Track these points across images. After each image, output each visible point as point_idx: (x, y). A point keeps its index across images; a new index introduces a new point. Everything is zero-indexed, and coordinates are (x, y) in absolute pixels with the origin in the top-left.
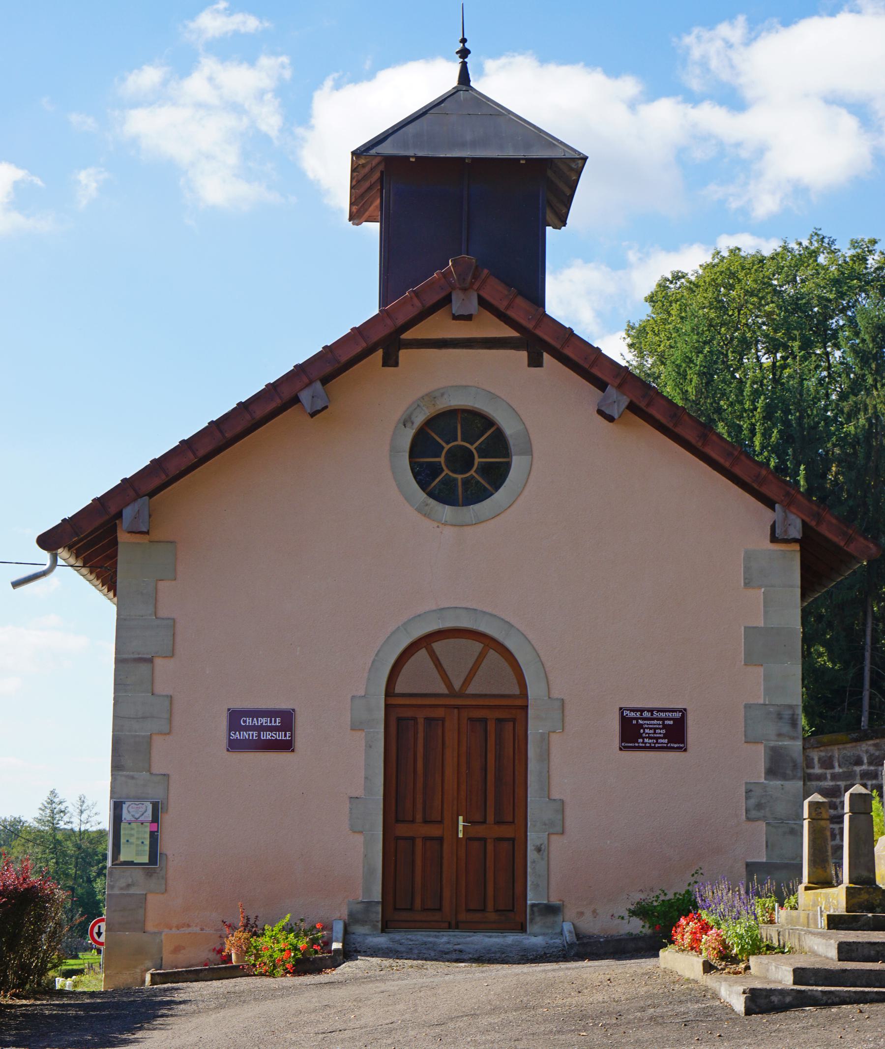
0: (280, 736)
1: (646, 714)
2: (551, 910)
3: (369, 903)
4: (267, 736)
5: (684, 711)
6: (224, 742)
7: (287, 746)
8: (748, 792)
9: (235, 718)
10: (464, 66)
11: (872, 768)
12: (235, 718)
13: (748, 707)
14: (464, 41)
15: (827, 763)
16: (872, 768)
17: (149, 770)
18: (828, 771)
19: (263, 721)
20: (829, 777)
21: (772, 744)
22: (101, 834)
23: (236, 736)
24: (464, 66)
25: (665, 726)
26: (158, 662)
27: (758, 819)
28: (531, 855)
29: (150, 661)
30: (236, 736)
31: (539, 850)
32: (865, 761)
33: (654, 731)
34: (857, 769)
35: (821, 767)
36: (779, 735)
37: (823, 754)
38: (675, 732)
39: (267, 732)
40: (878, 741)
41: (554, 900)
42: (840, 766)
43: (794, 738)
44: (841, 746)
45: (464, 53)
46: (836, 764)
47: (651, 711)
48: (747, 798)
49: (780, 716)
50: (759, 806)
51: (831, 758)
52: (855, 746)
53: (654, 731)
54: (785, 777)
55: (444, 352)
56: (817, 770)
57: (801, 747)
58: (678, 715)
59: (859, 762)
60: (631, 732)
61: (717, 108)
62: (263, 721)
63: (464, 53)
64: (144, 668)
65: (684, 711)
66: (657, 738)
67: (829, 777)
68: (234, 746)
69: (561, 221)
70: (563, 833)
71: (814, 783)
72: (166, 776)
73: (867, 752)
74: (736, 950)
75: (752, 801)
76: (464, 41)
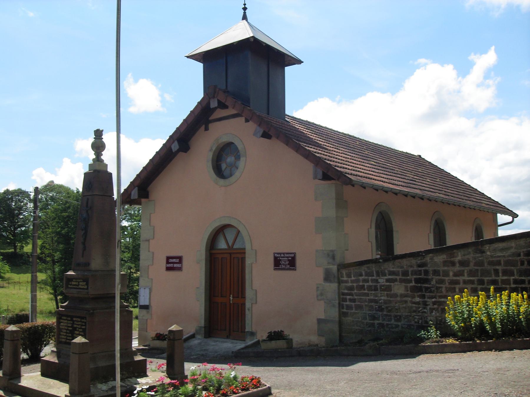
1: (282, 255)
2: (253, 334)
3: (201, 327)
5: (295, 254)
6: (165, 268)
8: (318, 288)
10: (245, 13)
11: (366, 278)
13: (317, 251)
15: (349, 276)
16: (366, 278)
17: (148, 277)
18: (349, 279)
20: (350, 281)
21: (326, 267)
24: (245, 13)
25: (289, 260)
26: (151, 241)
27: (320, 300)
28: (247, 311)
31: (249, 310)
32: (364, 274)
33: (285, 262)
34: (361, 278)
35: (346, 277)
36: (329, 263)
37: (347, 271)
38: (292, 263)
40: (368, 265)
41: (254, 330)
42: (354, 276)
43: (334, 265)
44: (354, 268)
46: (352, 276)
47: (284, 254)
48: (317, 291)
49: (328, 255)
50: (322, 294)
51: (350, 273)
52: (21, 311)
53: (285, 262)
54: (330, 281)
56: (345, 279)
57: (336, 269)
58: (293, 255)
59: (361, 275)
60: (277, 263)
64: (147, 243)
65: (295, 254)
66: (286, 265)
67: (350, 281)
68: (168, 269)
70: (256, 303)
71: (344, 284)
72: (152, 279)
73: (364, 270)
75: (319, 292)
76: (245, 4)
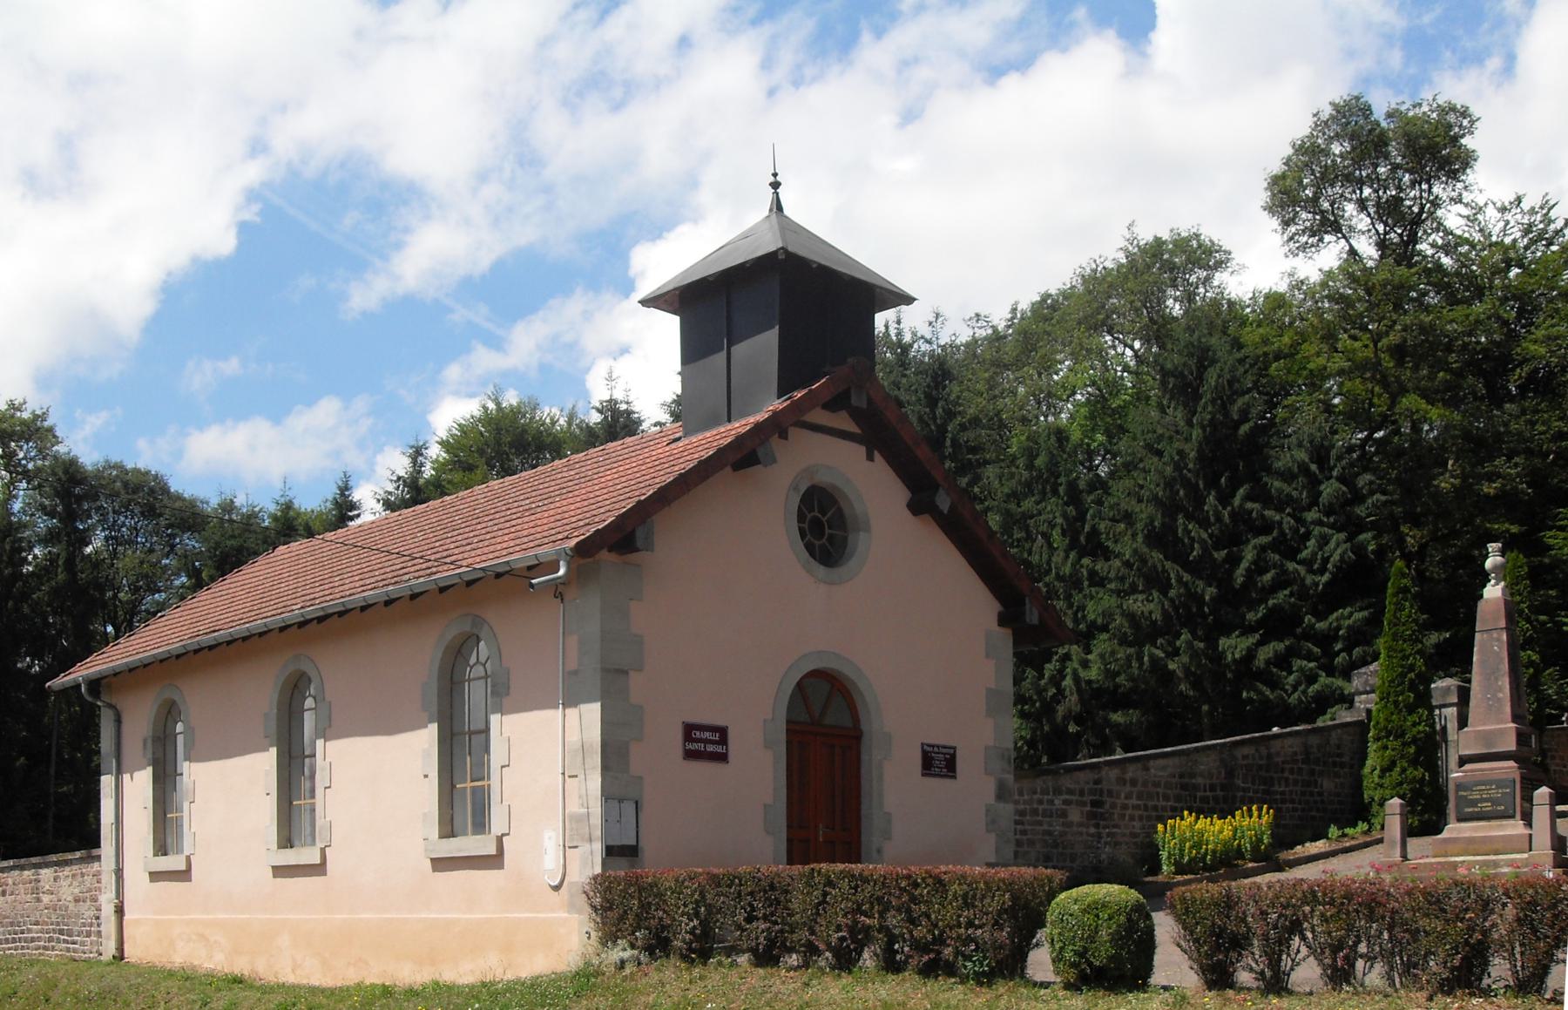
0: (719, 749)
4: (710, 748)
6: (680, 752)
7: (722, 758)
9: (689, 730)
12: (689, 730)
14: (775, 175)
19: (707, 735)
22: (325, 732)
23: (690, 746)
26: (631, 673)
29: (626, 673)
30: (690, 746)
39: (706, 743)
45: (776, 185)
55: (820, 435)
61: (1027, 299)
62: (707, 735)
63: (776, 185)
68: (690, 755)
69: (875, 295)
74: (1099, 621)
76: (775, 175)
